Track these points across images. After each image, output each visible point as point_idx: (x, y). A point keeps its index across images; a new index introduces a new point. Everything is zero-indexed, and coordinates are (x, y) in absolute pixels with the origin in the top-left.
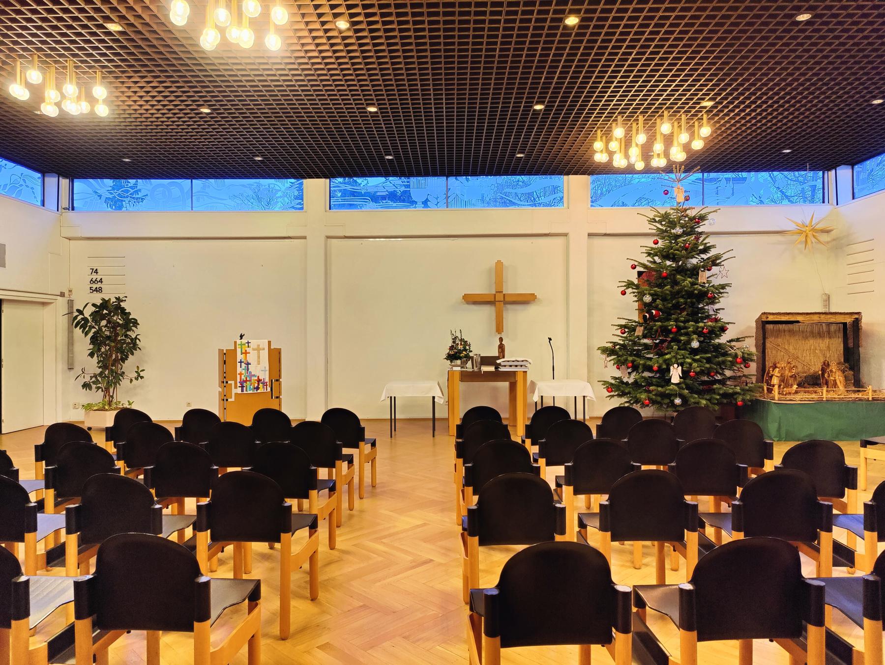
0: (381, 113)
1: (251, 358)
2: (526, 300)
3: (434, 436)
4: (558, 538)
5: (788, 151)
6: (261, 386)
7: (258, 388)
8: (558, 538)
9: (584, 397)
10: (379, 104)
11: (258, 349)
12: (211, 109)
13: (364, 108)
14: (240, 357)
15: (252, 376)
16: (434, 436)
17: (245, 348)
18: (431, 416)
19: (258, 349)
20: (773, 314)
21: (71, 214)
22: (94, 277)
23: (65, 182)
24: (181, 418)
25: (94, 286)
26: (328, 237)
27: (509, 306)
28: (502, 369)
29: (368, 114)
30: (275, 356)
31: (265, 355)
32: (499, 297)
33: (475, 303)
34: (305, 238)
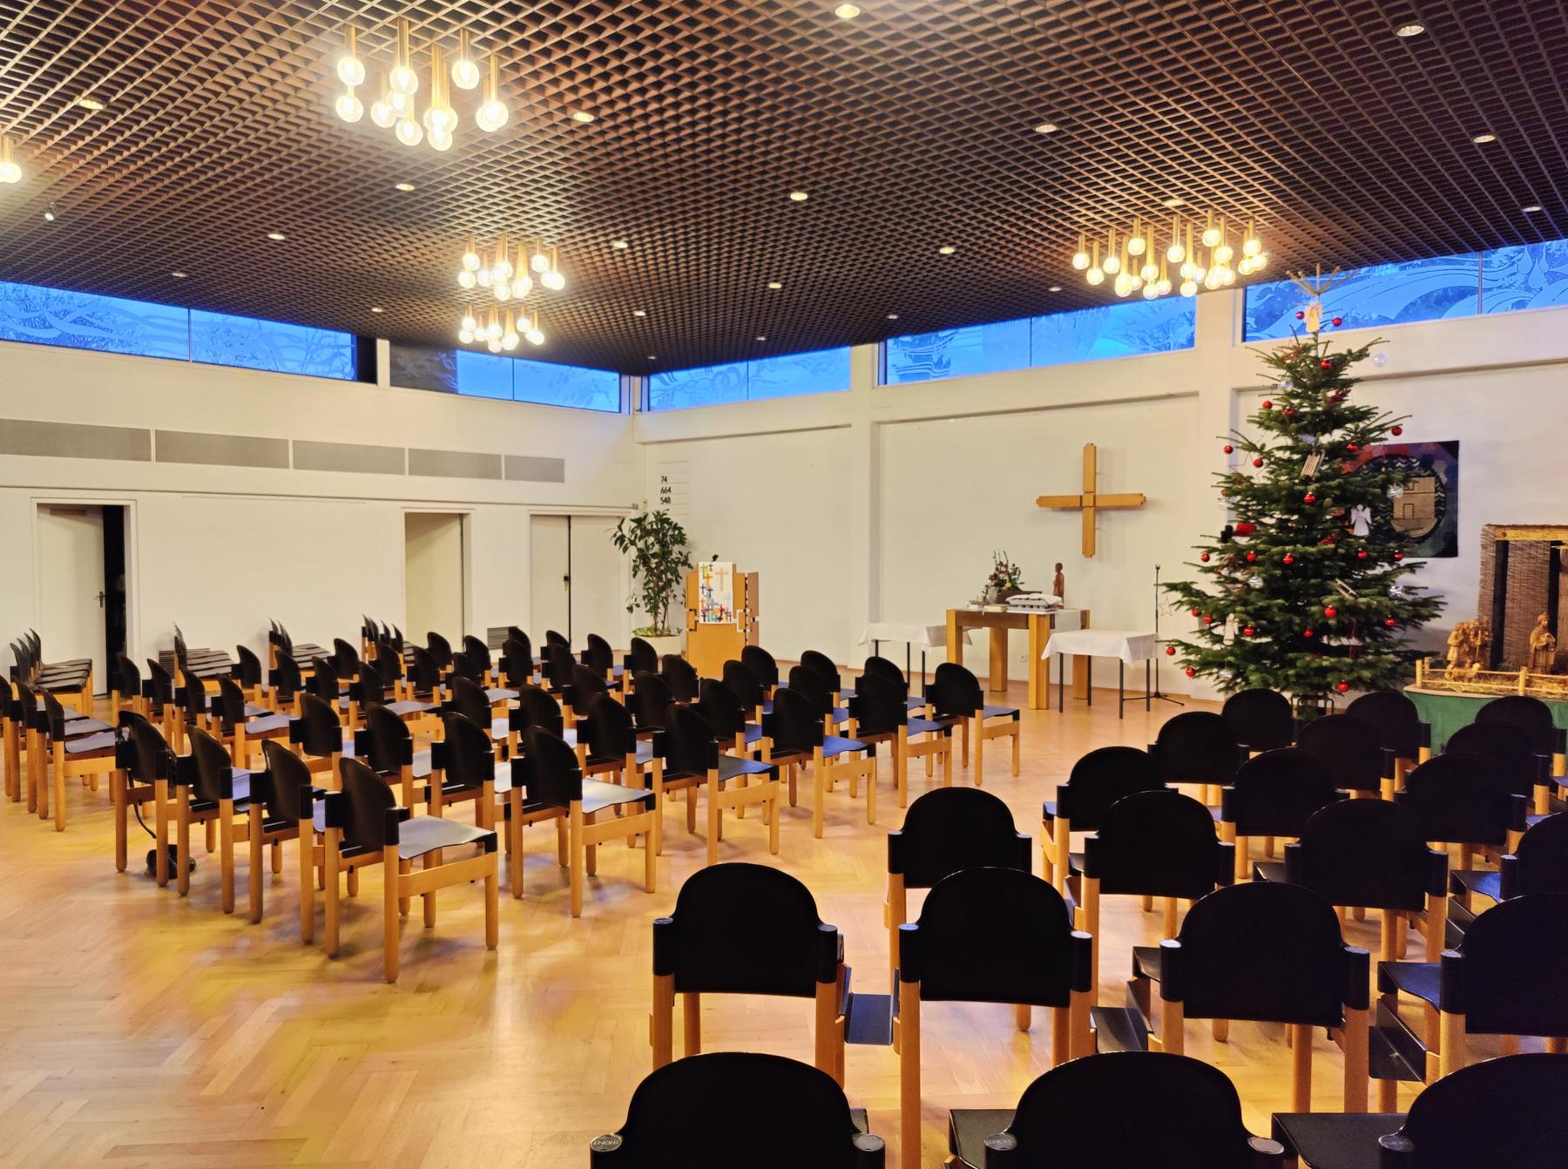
0: (1437, 32)
1: (714, 584)
2: (1138, 504)
3: (1121, 717)
4: (1092, 835)
5: (181, 275)
6: (724, 616)
7: (720, 619)
8: (1092, 835)
9: (877, 642)
10: (1427, 13)
11: (722, 573)
12: (1058, 124)
13: (1390, 34)
14: (702, 582)
15: (713, 604)
16: (1121, 717)
17: (707, 572)
18: (1118, 687)
19: (722, 573)
20: (1515, 527)
21: (645, 416)
22: (666, 485)
23: (637, 380)
24: (862, 667)
25: (665, 496)
26: (1239, 391)
27: (1113, 514)
28: (1011, 610)
29: (1403, 45)
30: (747, 586)
31: (729, 579)
32: (1088, 501)
33: (1065, 509)
34: (849, 426)
